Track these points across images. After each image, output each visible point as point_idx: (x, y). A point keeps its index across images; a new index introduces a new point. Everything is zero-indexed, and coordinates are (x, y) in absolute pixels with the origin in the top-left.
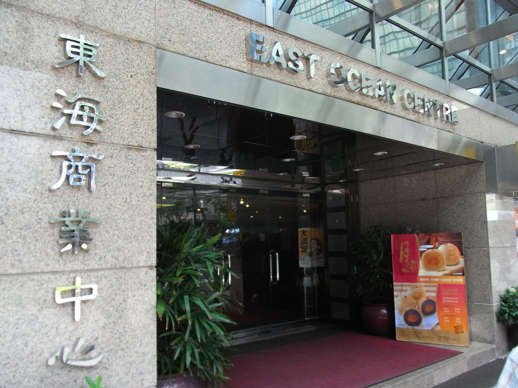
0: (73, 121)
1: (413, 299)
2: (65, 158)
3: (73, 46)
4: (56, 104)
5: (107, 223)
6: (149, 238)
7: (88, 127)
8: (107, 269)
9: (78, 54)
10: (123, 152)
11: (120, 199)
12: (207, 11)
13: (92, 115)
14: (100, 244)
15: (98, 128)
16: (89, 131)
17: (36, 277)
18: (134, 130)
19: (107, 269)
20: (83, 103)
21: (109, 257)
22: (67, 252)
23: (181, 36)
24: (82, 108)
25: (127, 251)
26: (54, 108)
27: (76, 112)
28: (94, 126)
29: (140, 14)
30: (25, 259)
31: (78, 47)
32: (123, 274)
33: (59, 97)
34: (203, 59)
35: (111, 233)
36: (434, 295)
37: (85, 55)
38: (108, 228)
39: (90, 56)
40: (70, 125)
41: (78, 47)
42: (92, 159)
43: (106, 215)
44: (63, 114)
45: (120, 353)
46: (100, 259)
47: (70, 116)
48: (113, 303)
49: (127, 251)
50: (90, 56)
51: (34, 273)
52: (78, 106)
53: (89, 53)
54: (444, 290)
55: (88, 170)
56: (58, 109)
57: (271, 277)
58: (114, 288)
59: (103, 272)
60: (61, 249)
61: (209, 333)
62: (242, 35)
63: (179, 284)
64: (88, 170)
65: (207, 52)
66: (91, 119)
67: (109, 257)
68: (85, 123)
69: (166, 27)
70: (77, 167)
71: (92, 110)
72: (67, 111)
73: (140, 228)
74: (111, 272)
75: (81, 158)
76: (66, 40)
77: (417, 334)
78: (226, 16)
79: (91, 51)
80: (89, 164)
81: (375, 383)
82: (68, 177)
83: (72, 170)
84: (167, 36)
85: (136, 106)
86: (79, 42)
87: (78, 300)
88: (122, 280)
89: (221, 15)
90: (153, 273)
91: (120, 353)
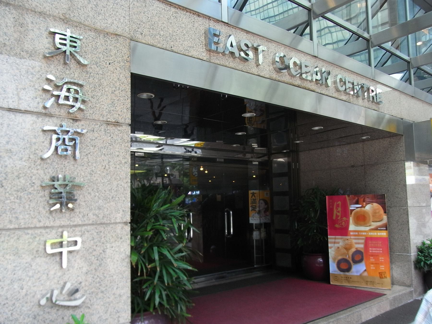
0: (61, 101)
1: (345, 250)
2: (55, 132)
3: (60, 39)
4: (47, 87)
5: (89, 186)
6: (124, 199)
7: (73, 106)
8: (89, 225)
9: (65, 45)
10: (103, 127)
11: (100, 166)
12: (173, 10)
13: (77, 96)
14: (83, 204)
15: (82, 107)
16: (75, 109)
17: (30, 231)
18: (112, 109)
19: (89, 225)
20: (69, 86)
21: (91, 215)
22: (56, 210)
23: (151, 30)
24: (69, 90)
25: (106, 210)
26: (45, 90)
27: (64, 93)
28: (78, 105)
29: (117, 12)
30: (21, 217)
31: (65, 40)
32: (103, 228)
33: (49, 81)
34: (170, 49)
35: (93, 194)
36: (362, 246)
37: (71, 46)
38: (90, 190)
39: (75, 47)
40: (59, 105)
41: (65, 40)
42: (76, 133)
43: (89, 180)
44: (53, 95)
45: (100, 295)
46: (84, 216)
47: (58, 97)
48: (94, 253)
49: (106, 210)
50: (75, 47)
51: (28, 228)
52: (65, 89)
53: (75, 44)
54: (370, 242)
55: (74, 142)
56: (48, 91)
57: (226, 231)
58: (95, 241)
59: (86, 227)
60: (51, 208)
61: (174, 278)
62: (202, 29)
63: (149, 237)
64: (74, 142)
65: (172, 43)
66: (76, 100)
67: (91, 215)
68: (71, 103)
69: (139, 23)
70: (64, 139)
71: (77, 92)
72: (56, 93)
73: (116, 191)
74: (92, 227)
75: (68, 132)
76: (55, 33)
77: (348, 279)
78: (188, 14)
79: (76, 42)
80: (74, 137)
81: (313, 320)
82: (56, 148)
83: (60, 142)
84: (139, 30)
85: (114, 89)
86: (65, 35)
87: (65, 250)
88: (102, 234)
89: (184, 13)
90: (128, 228)
91: (100, 295)
